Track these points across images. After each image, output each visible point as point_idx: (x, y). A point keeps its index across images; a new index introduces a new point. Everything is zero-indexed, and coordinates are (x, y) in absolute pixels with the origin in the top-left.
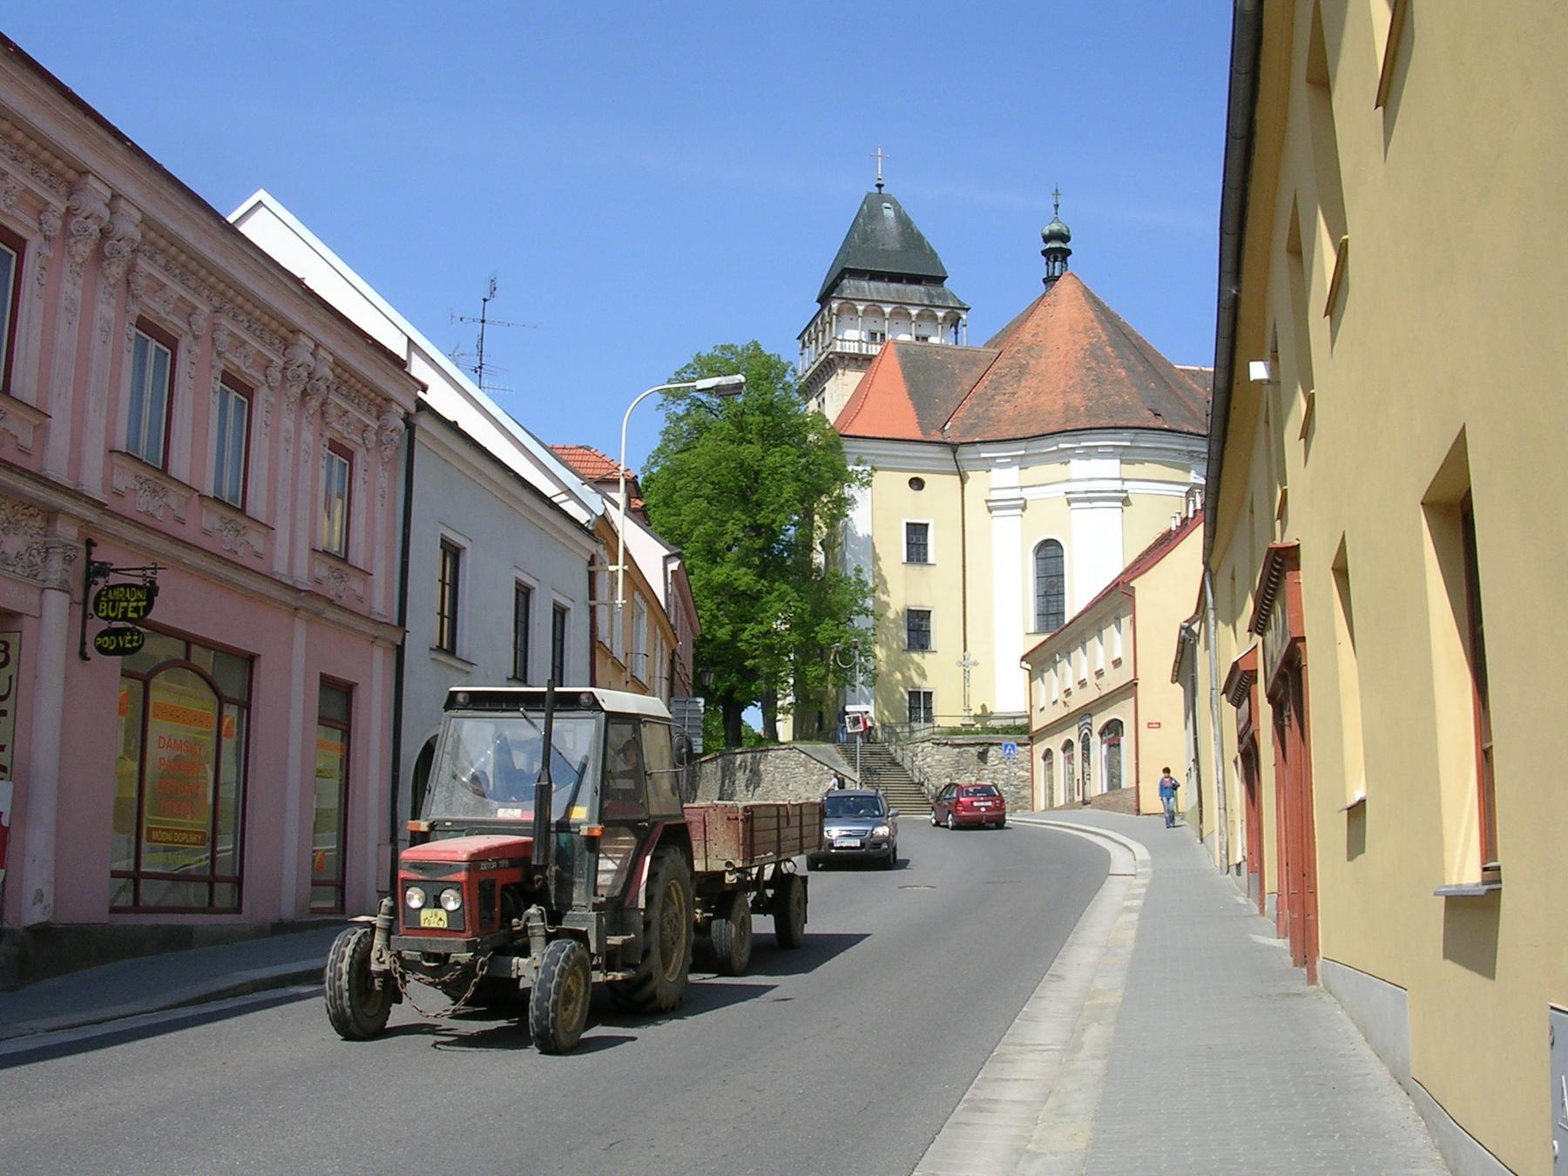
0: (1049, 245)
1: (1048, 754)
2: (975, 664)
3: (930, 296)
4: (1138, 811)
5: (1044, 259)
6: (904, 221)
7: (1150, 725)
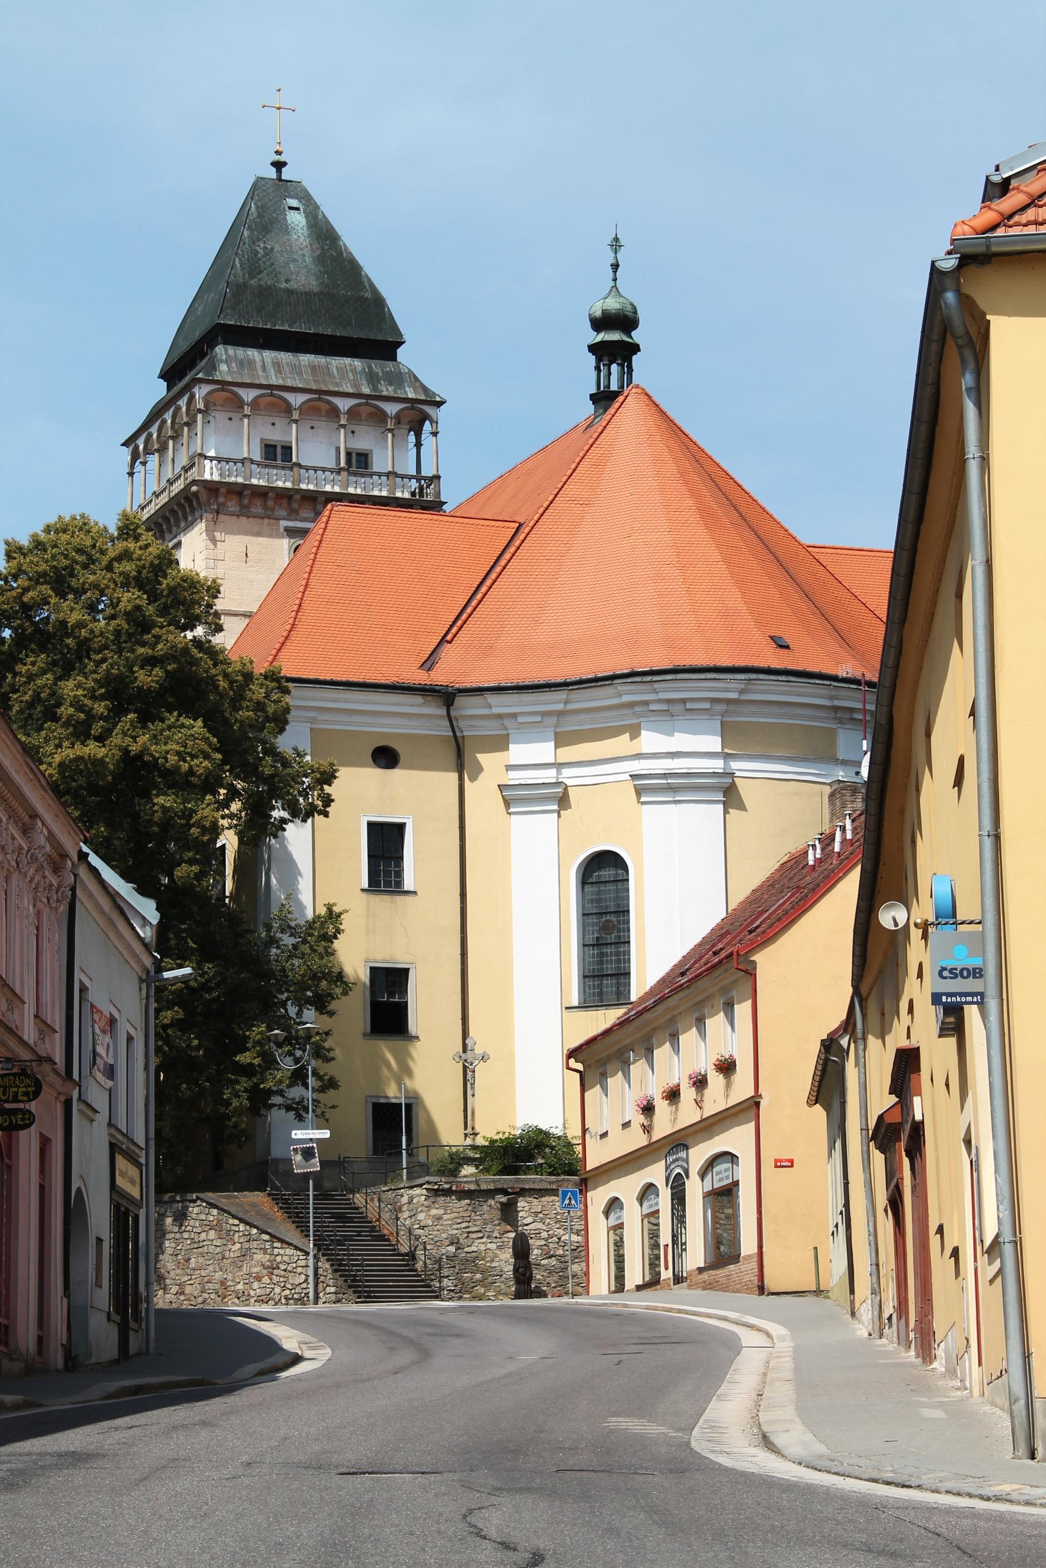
0: (602, 337)
1: (614, 1204)
2: (484, 1058)
3: (372, 379)
4: (761, 1289)
5: (592, 359)
6: (324, 235)
7: (778, 1164)
